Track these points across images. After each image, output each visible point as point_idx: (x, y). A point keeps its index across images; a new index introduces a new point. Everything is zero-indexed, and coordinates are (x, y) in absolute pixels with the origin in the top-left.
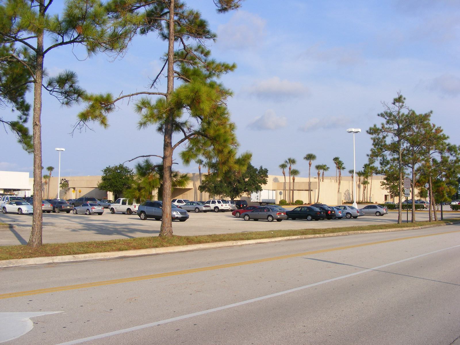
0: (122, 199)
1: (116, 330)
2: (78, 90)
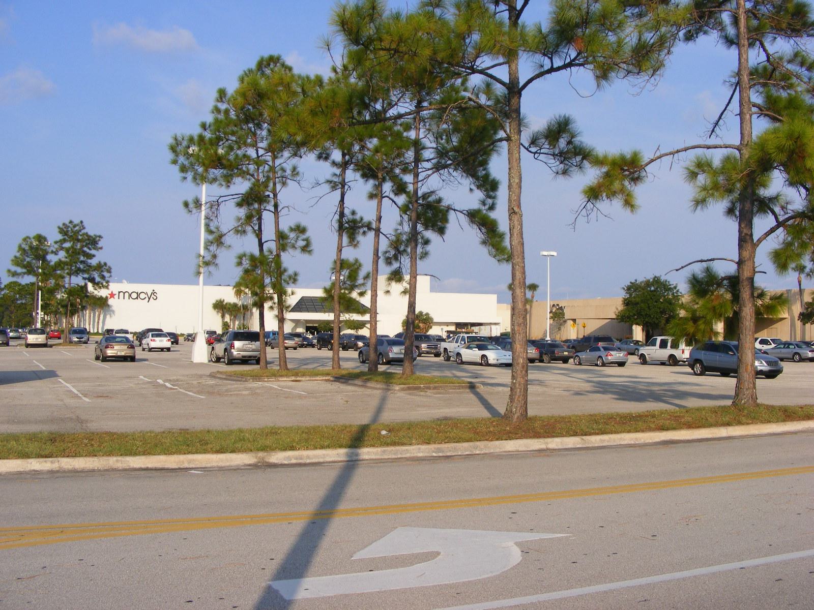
0: (659, 339)
1: (664, 573)
2: (581, 149)
